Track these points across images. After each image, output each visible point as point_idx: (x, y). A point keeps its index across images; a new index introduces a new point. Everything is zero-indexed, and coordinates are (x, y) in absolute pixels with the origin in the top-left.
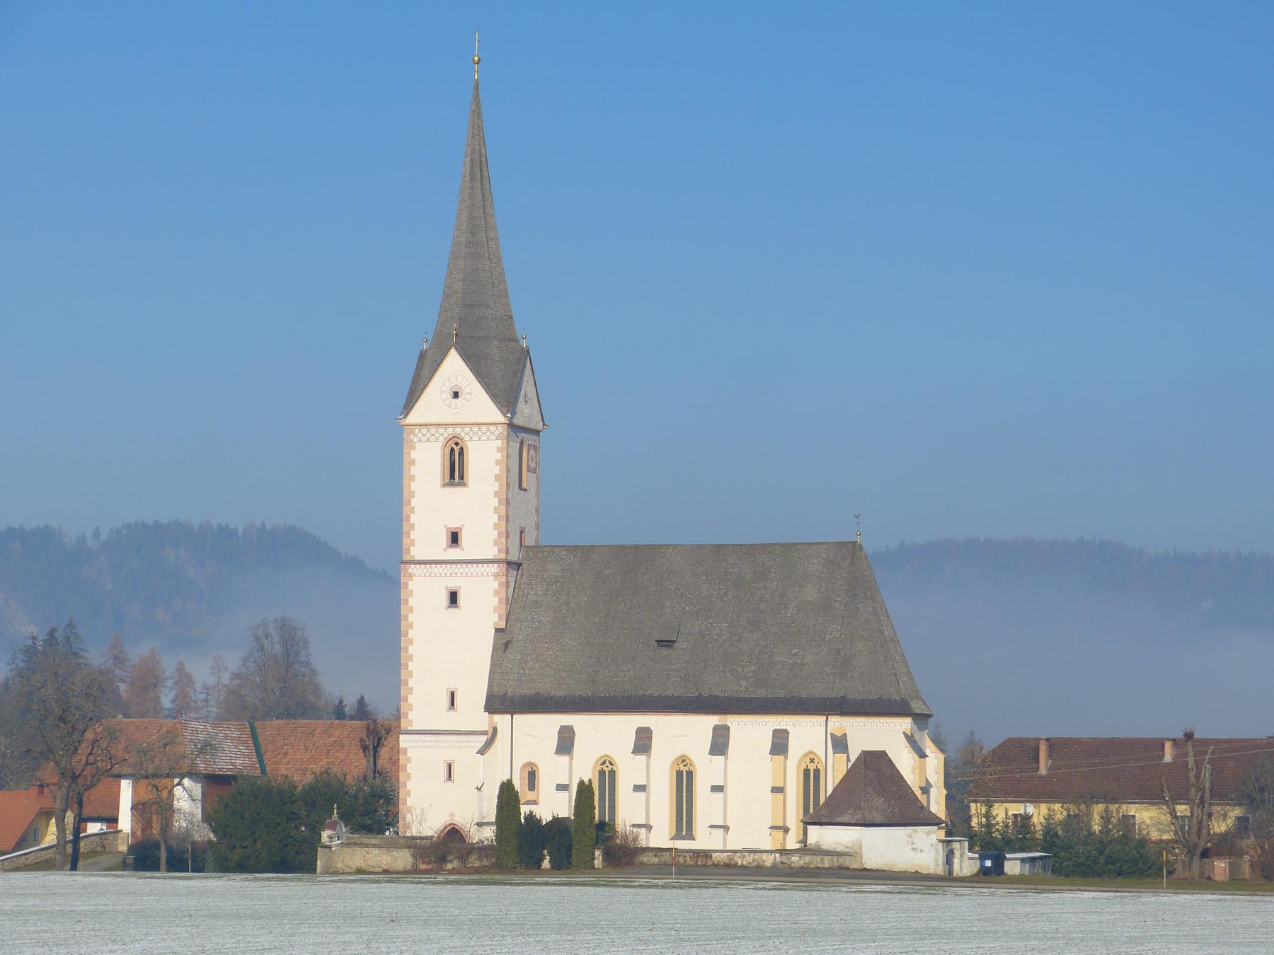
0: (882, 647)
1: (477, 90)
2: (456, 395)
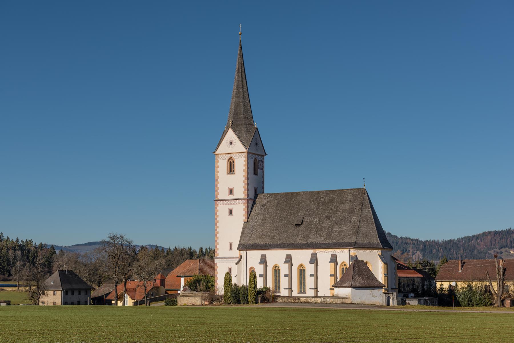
2: (231, 143)
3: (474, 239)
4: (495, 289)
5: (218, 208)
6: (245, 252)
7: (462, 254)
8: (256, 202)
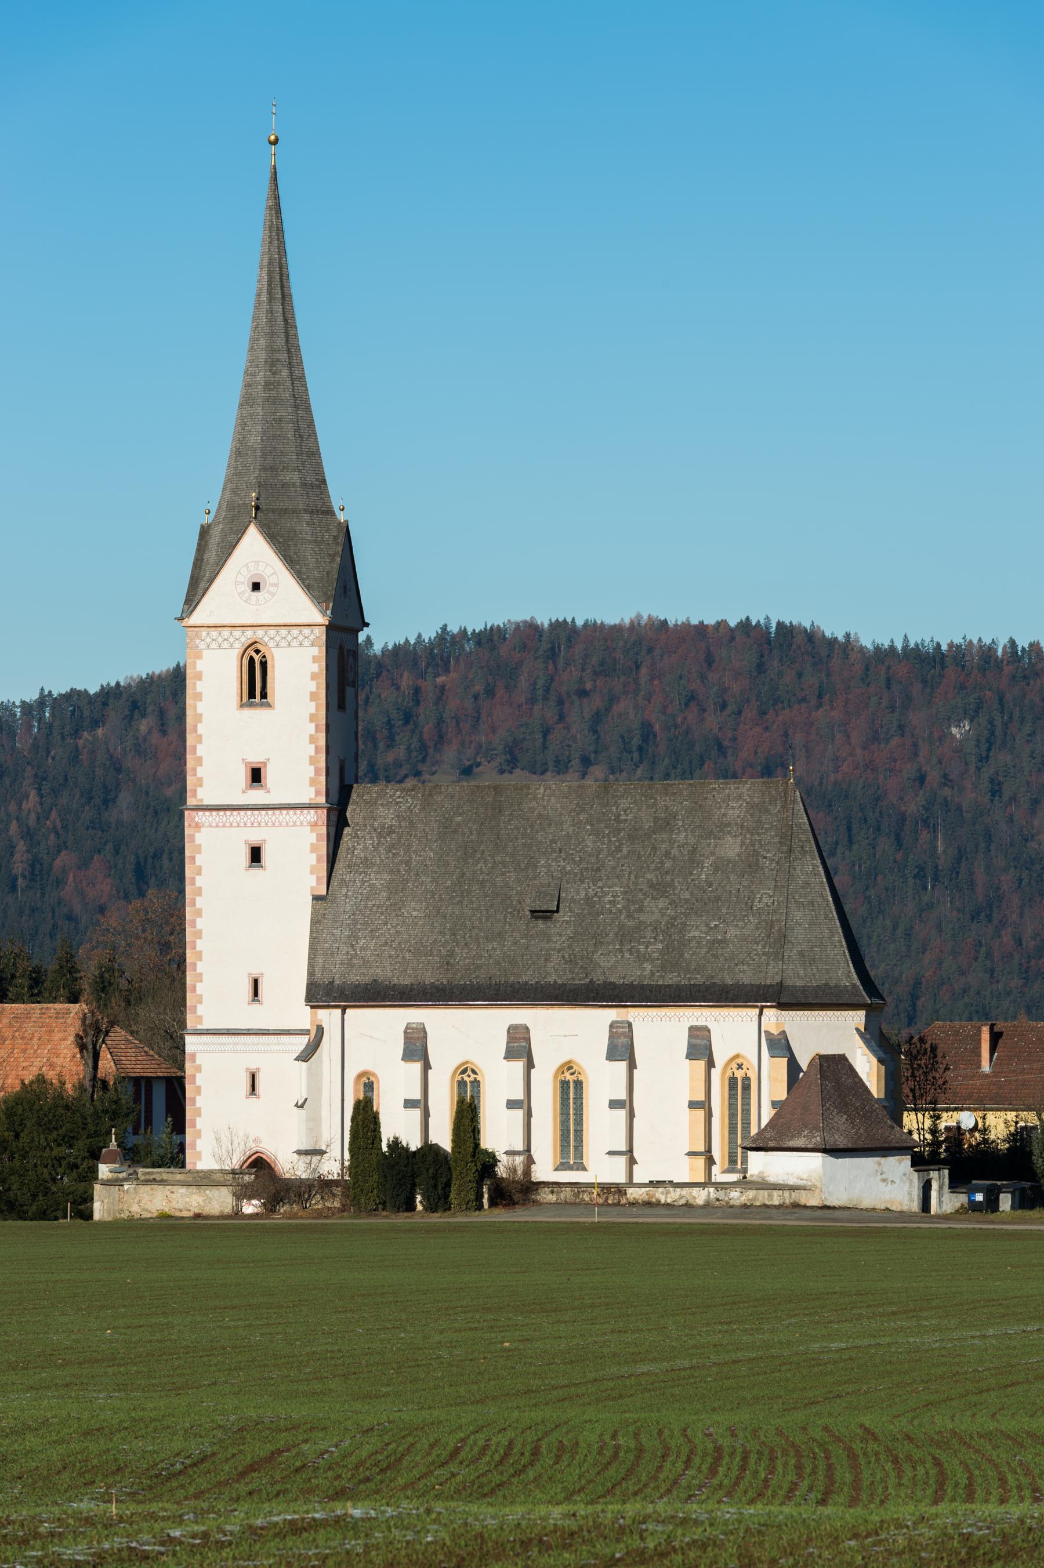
0: (826, 918)
7: (32, 821)
8: (348, 814)
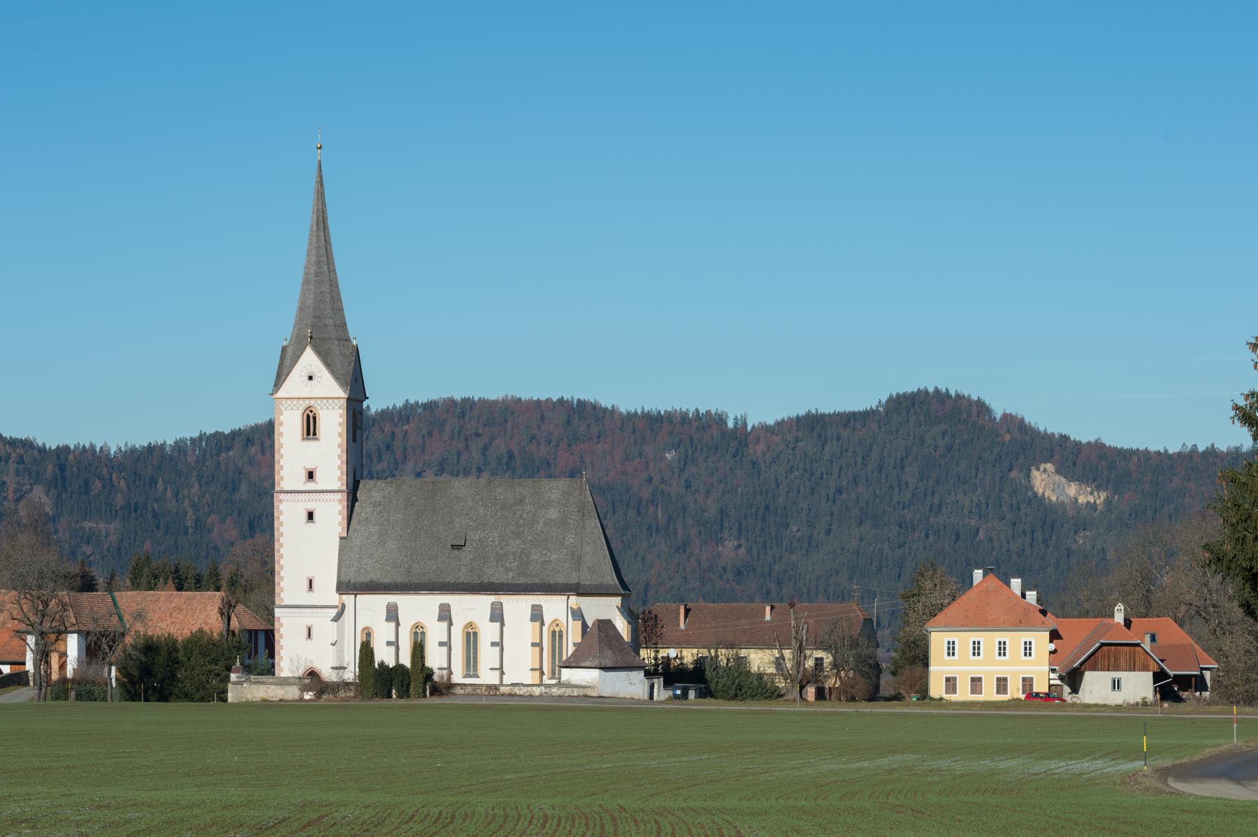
1: (320, 167)
2: (310, 378)
3: (238, 445)
4: (789, 665)
5: (282, 507)
6: (353, 596)
7: (196, 499)
